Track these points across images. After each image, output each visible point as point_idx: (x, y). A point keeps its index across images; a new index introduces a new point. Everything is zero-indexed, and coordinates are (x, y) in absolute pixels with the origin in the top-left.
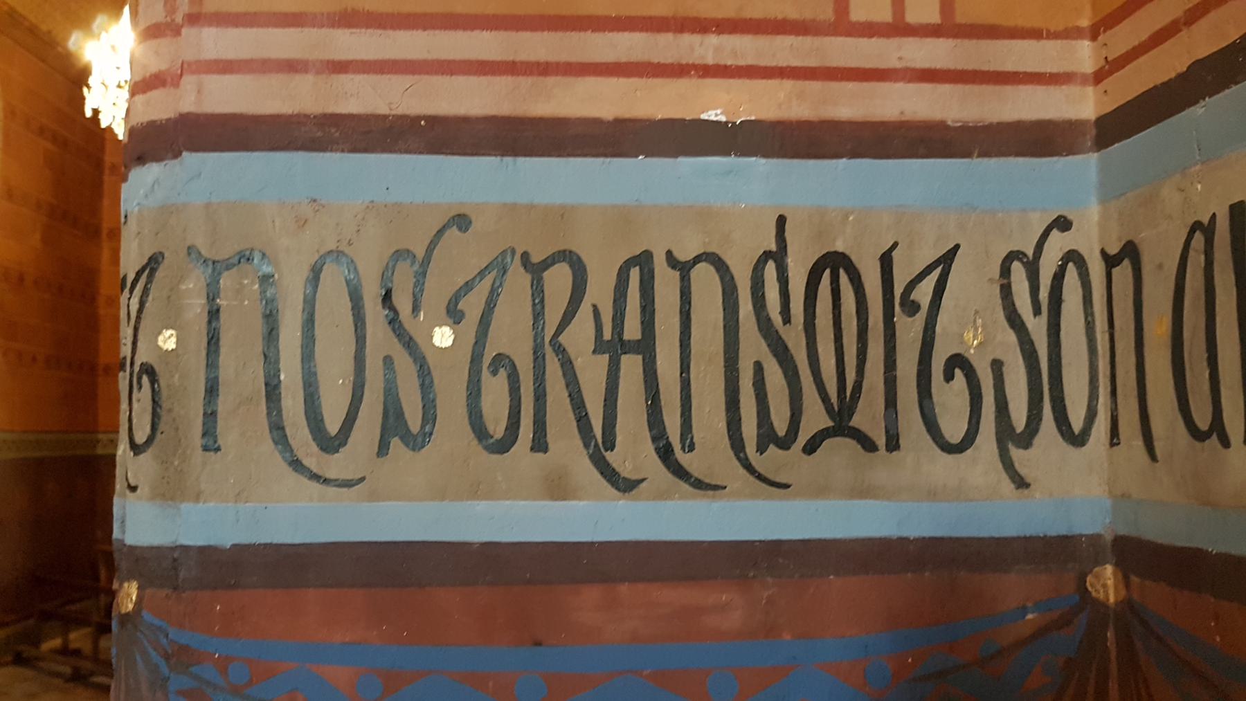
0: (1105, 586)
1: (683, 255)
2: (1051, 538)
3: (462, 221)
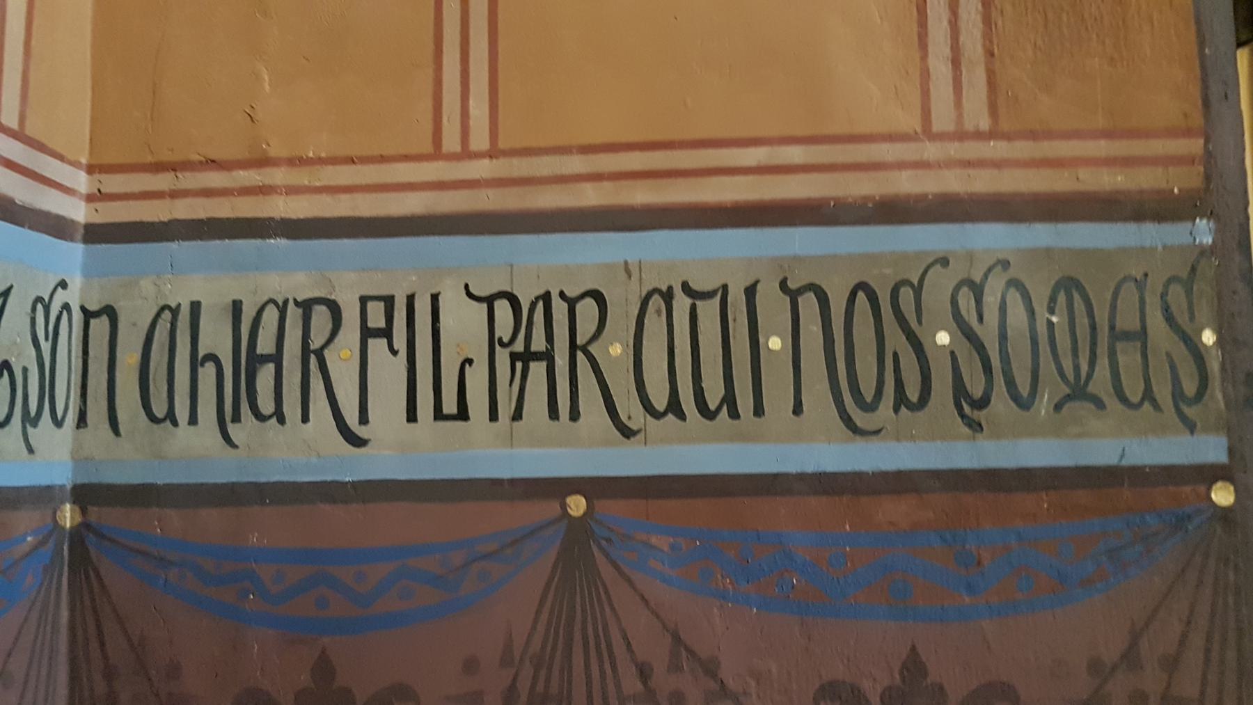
0: (65, 517)
1: (571, 293)
2: (43, 487)
3: (944, 262)
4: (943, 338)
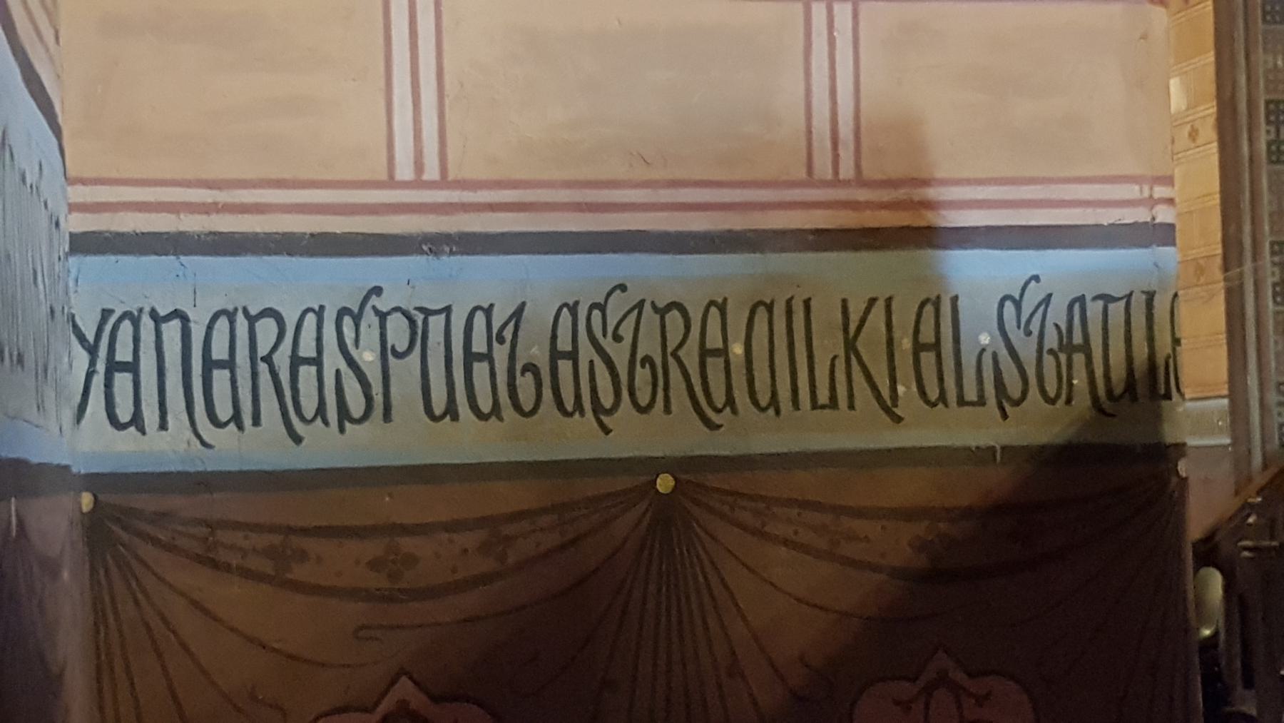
3: (623, 288)
4: (985, 339)
